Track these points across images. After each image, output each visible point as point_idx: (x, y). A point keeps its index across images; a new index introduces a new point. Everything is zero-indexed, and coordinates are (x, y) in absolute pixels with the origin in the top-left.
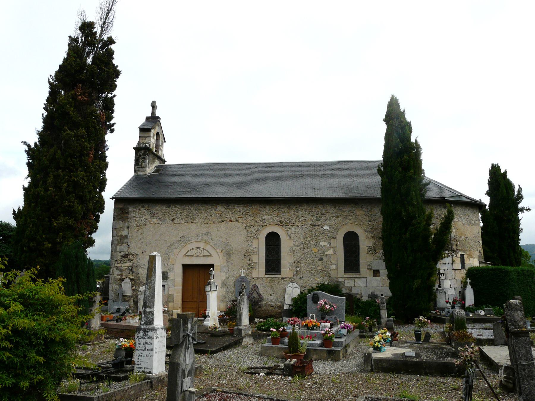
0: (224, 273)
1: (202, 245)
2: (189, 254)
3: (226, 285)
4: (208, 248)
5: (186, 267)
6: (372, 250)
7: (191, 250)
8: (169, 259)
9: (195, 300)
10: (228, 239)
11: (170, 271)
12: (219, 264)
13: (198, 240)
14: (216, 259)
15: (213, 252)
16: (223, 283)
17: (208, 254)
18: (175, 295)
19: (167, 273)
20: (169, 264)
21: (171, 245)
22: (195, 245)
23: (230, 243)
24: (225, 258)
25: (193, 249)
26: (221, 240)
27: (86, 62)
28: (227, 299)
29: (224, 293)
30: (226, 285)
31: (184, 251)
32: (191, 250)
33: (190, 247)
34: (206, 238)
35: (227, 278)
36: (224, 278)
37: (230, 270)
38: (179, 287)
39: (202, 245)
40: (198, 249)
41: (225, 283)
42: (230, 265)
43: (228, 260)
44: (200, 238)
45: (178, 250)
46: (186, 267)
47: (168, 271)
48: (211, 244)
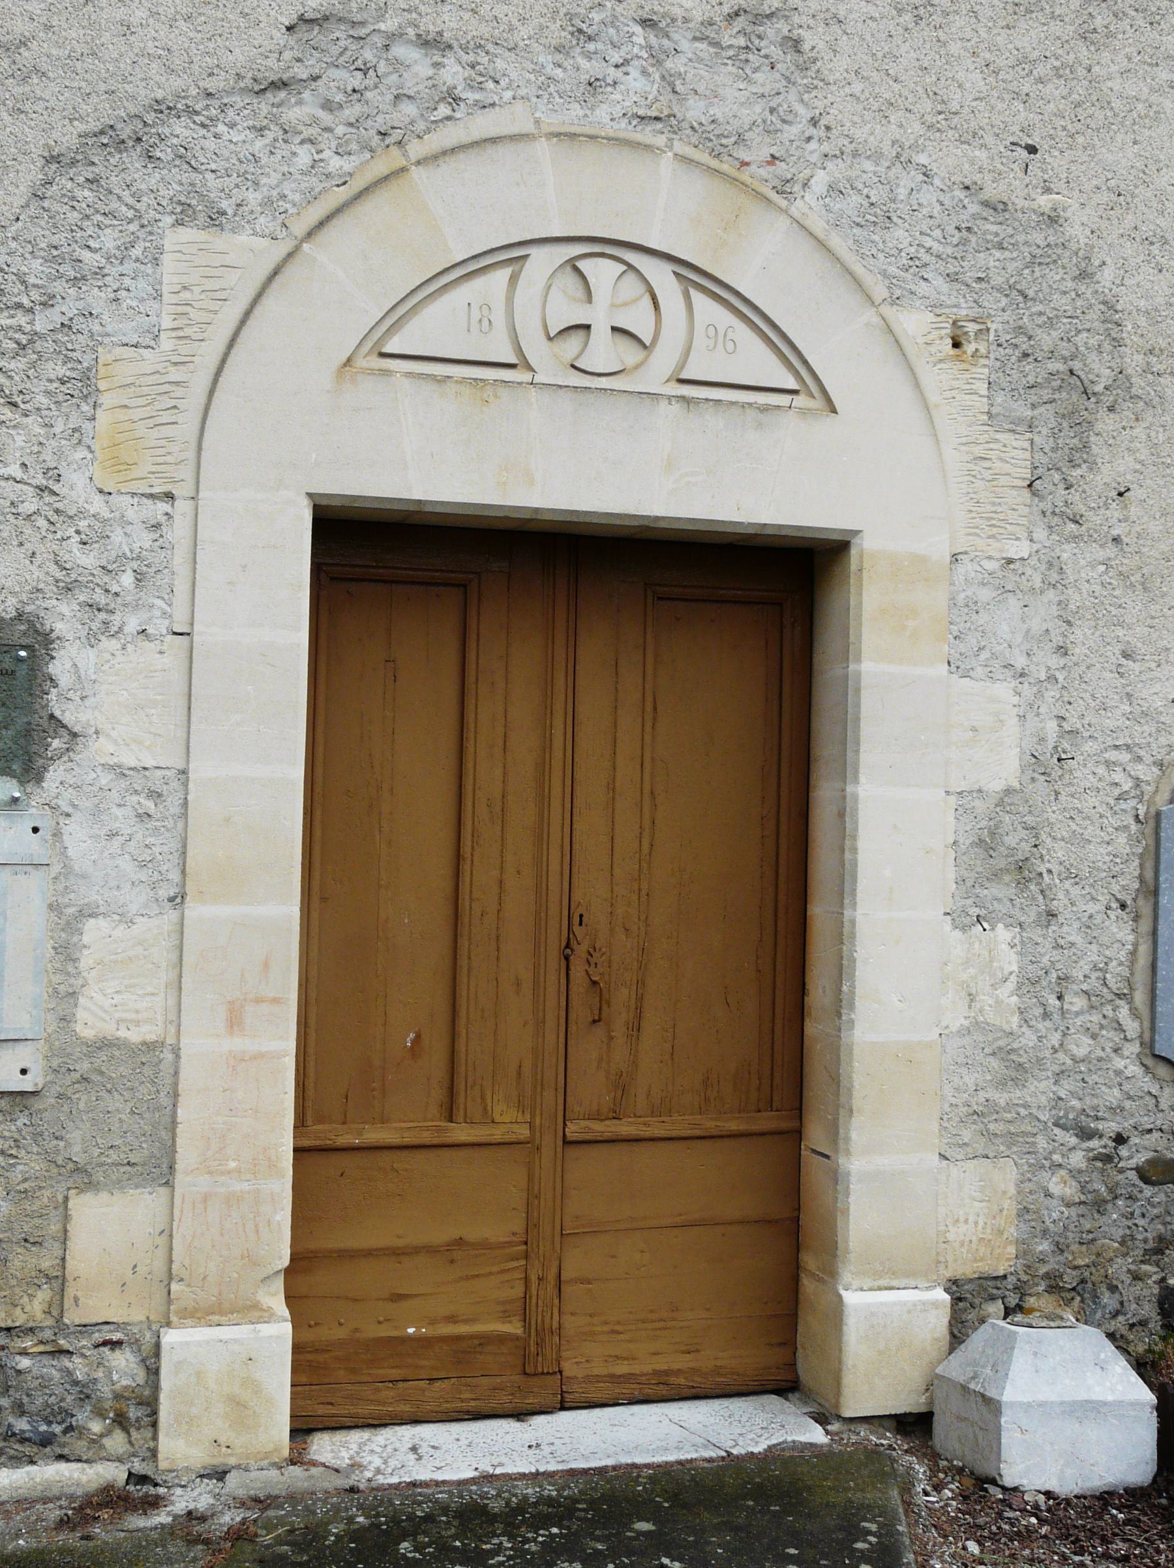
0: (1004, 690)
1: (664, 203)
2: (437, 328)
3: (1022, 871)
4: (764, 261)
5: (377, 562)
6: (589, 1130)
7: (475, 266)
8: (83, 386)
9: (509, 1122)
10: (1055, 162)
11: (101, 618)
12: (939, 548)
13: (604, 115)
14: (883, 464)
15: (837, 342)
16: (987, 843)
17: (756, 362)
18: (203, 1046)
19: (42, 642)
20: (77, 488)
21: (108, 138)
22: (548, 192)
23: (1076, 231)
24: (1014, 456)
25: (511, 255)
26: (948, 159)
27: (856, 1541)
28: (1039, 1091)
29: (1002, 1005)
30: (1022, 871)
31: (353, 276)
32: (475, 266)
33: (464, 206)
34: (726, 97)
35: (1049, 764)
36: (1001, 768)
37: (1083, 636)
38: (260, 915)
39: (664, 203)
40: (602, 272)
41: (1015, 839)
42: (1084, 562)
43: (1056, 481)
44: (637, 87)
45: (247, 251)
46: (377, 562)
47: (63, 617)
48: (809, 205)
